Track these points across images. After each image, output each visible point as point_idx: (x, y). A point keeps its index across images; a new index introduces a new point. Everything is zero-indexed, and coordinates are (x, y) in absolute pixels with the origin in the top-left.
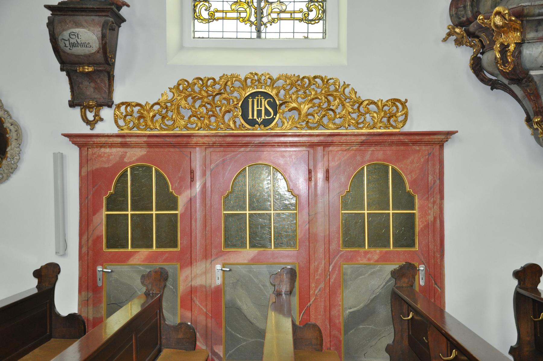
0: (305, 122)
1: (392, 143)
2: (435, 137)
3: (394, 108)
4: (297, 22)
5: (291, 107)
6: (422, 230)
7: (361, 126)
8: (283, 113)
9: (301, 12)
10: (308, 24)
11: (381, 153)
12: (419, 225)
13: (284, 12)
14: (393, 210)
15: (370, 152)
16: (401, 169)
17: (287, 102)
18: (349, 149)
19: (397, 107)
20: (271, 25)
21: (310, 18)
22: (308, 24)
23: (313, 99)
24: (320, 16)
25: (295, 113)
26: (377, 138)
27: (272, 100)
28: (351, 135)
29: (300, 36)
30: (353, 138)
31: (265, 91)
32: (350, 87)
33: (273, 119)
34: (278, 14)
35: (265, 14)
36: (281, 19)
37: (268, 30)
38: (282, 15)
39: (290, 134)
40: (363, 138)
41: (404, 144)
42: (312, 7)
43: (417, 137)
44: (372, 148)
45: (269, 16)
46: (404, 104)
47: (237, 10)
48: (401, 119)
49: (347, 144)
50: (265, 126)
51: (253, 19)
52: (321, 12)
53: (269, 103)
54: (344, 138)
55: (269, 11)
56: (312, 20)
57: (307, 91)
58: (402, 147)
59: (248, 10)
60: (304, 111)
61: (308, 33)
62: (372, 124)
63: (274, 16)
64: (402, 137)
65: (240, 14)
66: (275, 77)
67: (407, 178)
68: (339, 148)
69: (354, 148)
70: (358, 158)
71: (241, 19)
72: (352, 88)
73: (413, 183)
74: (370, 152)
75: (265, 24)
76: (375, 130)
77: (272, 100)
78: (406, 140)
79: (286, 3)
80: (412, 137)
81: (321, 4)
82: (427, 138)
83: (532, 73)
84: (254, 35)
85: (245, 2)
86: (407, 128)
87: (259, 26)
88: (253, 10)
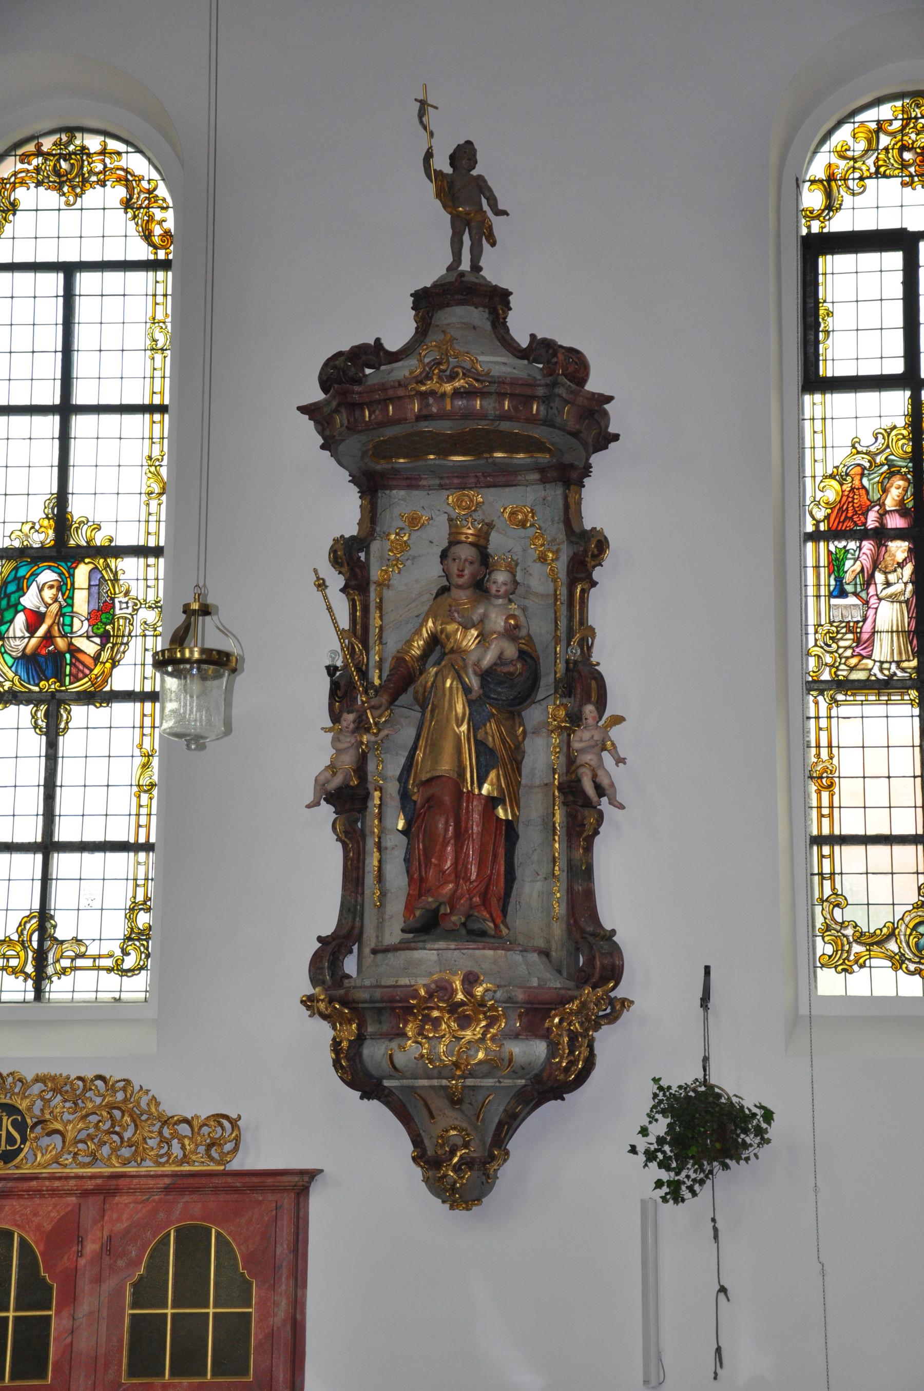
0: (72, 1155)
1: (216, 1190)
2: (285, 1178)
3: (219, 1129)
4: (103, 973)
5: (49, 1130)
6: (259, 1345)
7: (163, 1160)
8: (37, 1139)
9: (111, 956)
10: (121, 976)
11: (200, 1205)
12: (256, 1334)
13: (82, 956)
14: (207, 1306)
15: (180, 1205)
16: (230, 1234)
17: (45, 1121)
18: (147, 1200)
19: (224, 1129)
20: (59, 978)
21: (126, 966)
22: (121, 976)
23: (87, 1115)
24: (142, 963)
25: (57, 1139)
26: (191, 1180)
27: (19, 1118)
28: (145, 1176)
29: (107, 996)
30: (151, 1182)
31: (10, 1102)
32: (150, 1094)
33: (20, 1150)
34: (73, 960)
35: (50, 960)
36: (76, 969)
37: (54, 987)
38: (80, 962)
39: (44, 1175)
40: (167, 1181)
41: (235, 1190)
42: (129, 948)
43: (255, 1180)
44: (186, 1198)
45: (57, 965)
46: (234, 1123)
47: (4, 954)
48: (229, 1147)
49: (143, 1191)
50: (5, 1163)
51: (30, 969)
52: (143, 956)
53: (15, 1124)
54: (136, 1181)
55: (58, 956)
56: (129, 970)
57: (80, 1101)
58: (236, 1196)
59: (22, 954)
60: (70, 1136)
61: (121, 991)
62: (181, 1156)
63: (65, 963)
64: (230, 1180)
65: (8, 961)
66: (30, 1077)
67: (240, 1250)
68: (132, 1198)
69: (156, 1197)
70: (161, 1216)
71: (11, 969)
72: (153, 1096)
73: (249, 1259)
74: (180, 1205)
75: (50, 978)
76: (186, 1168)
77: (19, 1118)
78: (238, 1184)
79: (87, 943)
80: (247, 1179)
81: (145, 943)
82: (270, 1181)
83: (386, 1083)
84: (31, 996)
85: (18, 941)
86: (236, 1164)
87: (40, 979)
88: (30, 954)
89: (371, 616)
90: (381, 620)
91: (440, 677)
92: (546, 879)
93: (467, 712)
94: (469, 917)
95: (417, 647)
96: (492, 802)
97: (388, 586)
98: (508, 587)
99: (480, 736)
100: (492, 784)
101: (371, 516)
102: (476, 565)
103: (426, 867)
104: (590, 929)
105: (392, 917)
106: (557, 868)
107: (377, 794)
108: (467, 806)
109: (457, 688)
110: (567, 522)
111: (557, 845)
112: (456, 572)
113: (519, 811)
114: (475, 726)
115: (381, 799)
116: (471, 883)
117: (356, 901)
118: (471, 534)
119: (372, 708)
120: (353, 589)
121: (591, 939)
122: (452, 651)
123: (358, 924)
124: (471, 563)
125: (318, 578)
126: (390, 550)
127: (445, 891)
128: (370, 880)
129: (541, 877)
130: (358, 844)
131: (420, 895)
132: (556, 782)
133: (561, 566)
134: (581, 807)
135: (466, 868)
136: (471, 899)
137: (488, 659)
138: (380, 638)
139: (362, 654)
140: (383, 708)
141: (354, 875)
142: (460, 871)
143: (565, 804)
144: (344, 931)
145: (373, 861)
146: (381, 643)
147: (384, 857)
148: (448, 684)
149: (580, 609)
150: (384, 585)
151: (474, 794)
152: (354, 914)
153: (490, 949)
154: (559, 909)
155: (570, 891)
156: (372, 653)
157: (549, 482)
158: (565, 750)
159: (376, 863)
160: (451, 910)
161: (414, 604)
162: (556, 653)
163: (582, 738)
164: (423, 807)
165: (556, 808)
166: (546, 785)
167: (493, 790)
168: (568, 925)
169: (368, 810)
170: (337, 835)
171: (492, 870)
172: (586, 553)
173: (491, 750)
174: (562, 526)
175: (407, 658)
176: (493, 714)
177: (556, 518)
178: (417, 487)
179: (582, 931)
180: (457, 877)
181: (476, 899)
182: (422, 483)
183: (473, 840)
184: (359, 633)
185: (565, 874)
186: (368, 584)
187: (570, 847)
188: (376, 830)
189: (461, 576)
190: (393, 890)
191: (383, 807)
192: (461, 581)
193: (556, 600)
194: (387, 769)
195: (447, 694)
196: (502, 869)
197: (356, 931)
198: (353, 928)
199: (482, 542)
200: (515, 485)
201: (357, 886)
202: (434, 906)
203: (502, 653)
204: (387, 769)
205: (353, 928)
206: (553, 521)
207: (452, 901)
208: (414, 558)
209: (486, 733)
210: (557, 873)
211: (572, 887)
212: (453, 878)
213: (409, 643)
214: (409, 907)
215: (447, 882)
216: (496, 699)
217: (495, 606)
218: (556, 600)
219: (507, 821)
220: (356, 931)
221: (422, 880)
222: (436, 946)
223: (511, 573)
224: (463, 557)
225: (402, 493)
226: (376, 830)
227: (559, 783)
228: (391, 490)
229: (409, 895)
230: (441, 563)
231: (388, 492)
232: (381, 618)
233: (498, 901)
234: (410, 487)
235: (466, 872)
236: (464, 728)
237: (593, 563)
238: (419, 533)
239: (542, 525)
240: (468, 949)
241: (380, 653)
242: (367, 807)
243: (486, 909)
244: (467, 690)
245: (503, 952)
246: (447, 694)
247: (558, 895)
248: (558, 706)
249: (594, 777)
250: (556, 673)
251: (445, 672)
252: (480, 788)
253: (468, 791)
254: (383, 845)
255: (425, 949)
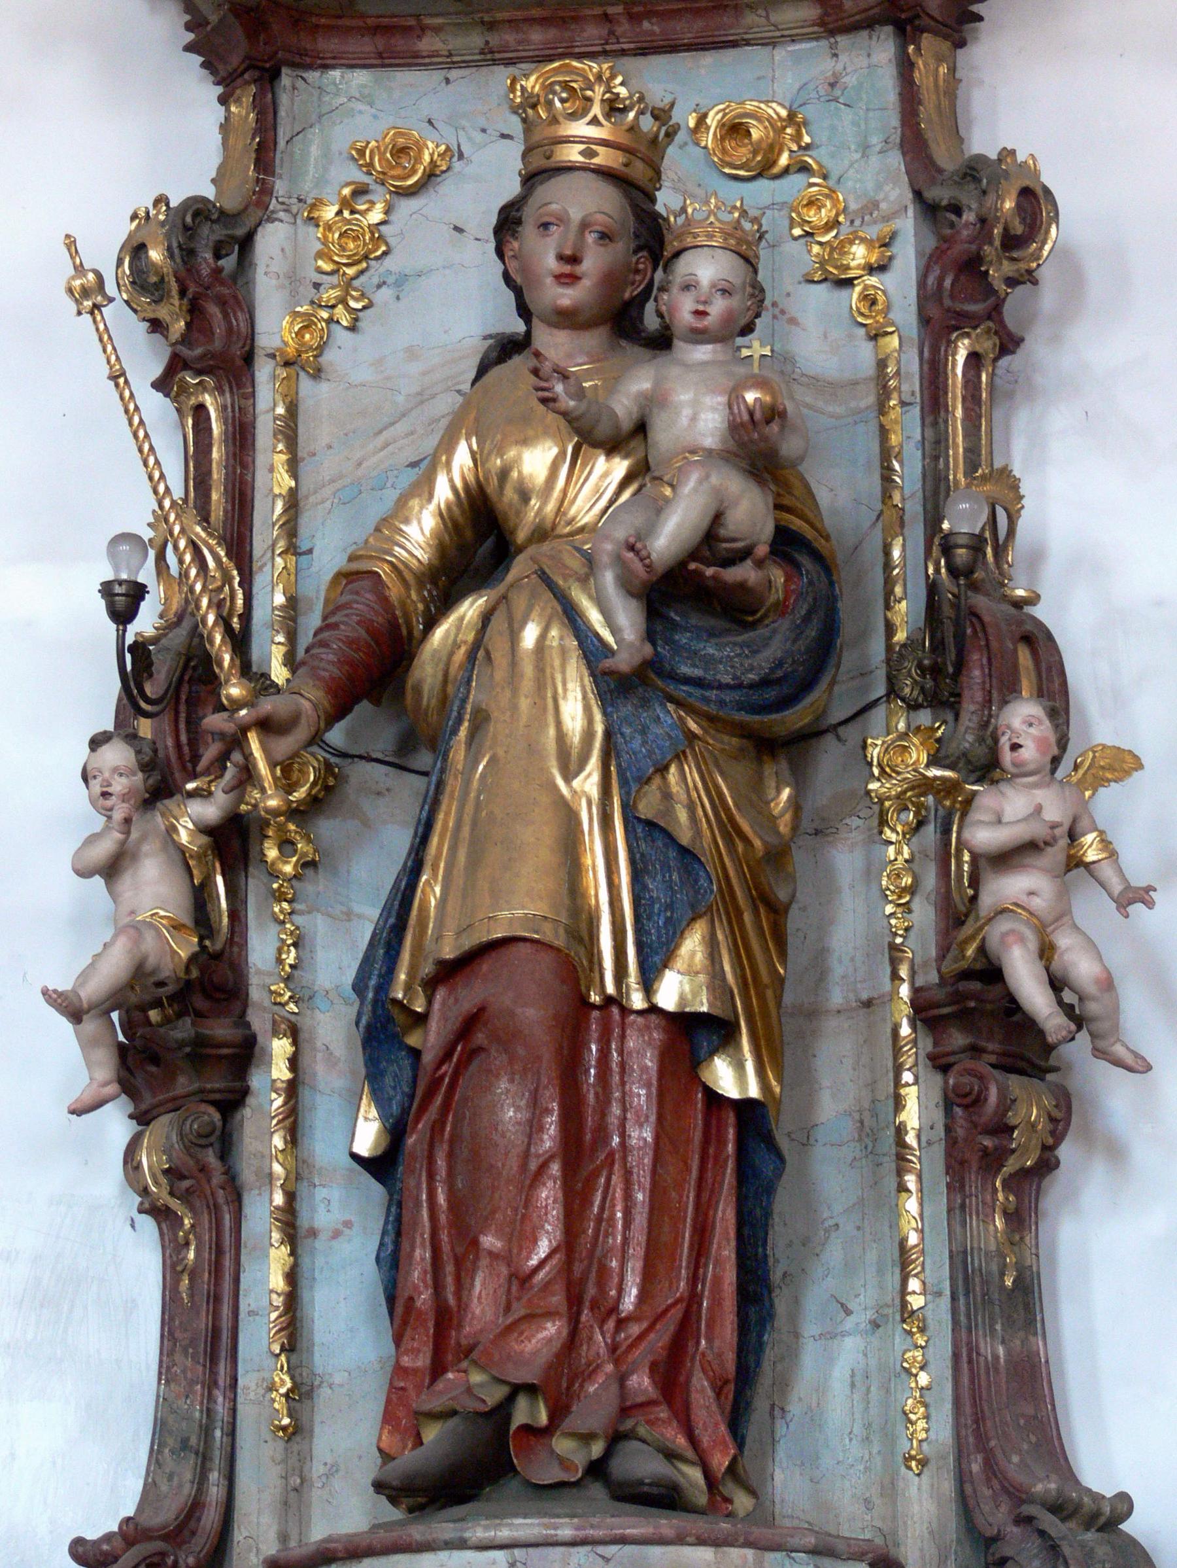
89: (261, 459)
90: (294, 474)
91: (498, 622)
92: (875, 1325)
93: (599, 728)
94: (616, 1438)
95: (419, 535)
96: (691, 1037)
97: (317, 374)
98: (735, 302)
99: (647, 808)
100: (690, 972)
101: (261, 150)
102: (620, 248)
103: (459, 1262)
104: (1045, 1486)
105: (332, 1470)
106: (914, 1284)
107: (281, 1048)
108: (604, 1054)
109: (563, 651)
110: (913, 143)
111: (912, 1205)
112: (551, 262)
113: (780, 1081)
114: (627, 774)
115: (294, 1063)
116: (621, 1323)
117: (210, 1412)
118: (604, 143)
119: (266, 726)
120: (199, 372)
121: (1048, 1521)
122: (542, 534)
123: (215, 1492)
124: (605, 237)
125: (80, 270)
126: (320, 255)
127: (529, 1347)
128: (258, 1338)
129: (861, 1318)
130: (215, 1210)
131: (437, 1369)
132: (905, 991)
133: (900, 286)
134: (1005, 1063)
135: (603, 1270)
136: (622, 1379)
137: (670, 535)
138: (291, 528)
139: (227, 579)
140: (301, 733)
141: (202, 1322)
142: (580, 1285)
143: (940, 1063)
144: (167, 1514)
145: (267, 1272)
146: (292, 549)
147: (305, 1262)
148: (530, 635)
149: (967, 417)
150: (302, 364)
151: (625, 1011)
152: (204, 1459)
153: (701, 1542)
154: (932, 1428)
155: (964, 1357)
156: (260, 582)
157: (851, 28)
158: (930, 880)
159: (277, 1282)
160: (552, 1417)
161: (401, 428)
162: (888, 565)
163: (1004, 814)
164: (447, 1055)
165: (907, 1077)
166: (868, 1004)
167: (695, 994)
168: (962, 1477)
169: (251, 1101)
170: (144, 1192)
171: (694, 1279)
172: (984, 255)
173: (684, 851)
174: (896, 160)
175: (383, 570)
176: (691, 737)
177: (875, 140)
178: (413, 60)
179: (1017, 1495)
180: (575, 1301)
181: (641, 1382)
182: (426, 44)
183: (627, 1174)
184: (222, 502)
185: (945, 1302)
186: (249, 358)
187: (958, 1210)
188: (277, 1169)
189: (569, 279)
190: (338, 1379)
191: (305, 1094)
192: (567, 297)
193: (884, 393)
194: (311, 953)
195: (528, 669)
196: (730, 1276)
197: (210, 1518)
198: (195, 1507)
199: (639, 172)
200: (734, 44)
201: (213, 1359)
202: (494, 1396)
203: (718, 518)
204: (311, 953)
205: (195, 1507)
206: (865, 148)
207: (559, 1385)
208: (401, 281)
209: (667, 796)
210: (916, 1302)
211: (973, 1349)
212: (557, 1299)
213: (389, 525)
214: (401, 1414)
215: (533, 1318)
216: (698, 683)
217: (688, 367)
218: (884, 393)
219: (745, 1107)
220: (210, 1518)
221: (445, 1319)
222: (504, 1534)
223: (747, 260)
224: (576, 215)
225: (360, 77)
226: (277, 1169)
227: (916, 991)
228: (325, 67)
229: (399, 1370)
230: (500, 253)
231: (313, 76)
232: (293, 467)
233: (718, 1394)
234: (385, 60)
235: (601, 1285)
236: (589, 782)
237: (1008, 268)
238: (413, 204)
239: (826, 161)
240: (623, 1540)
241: (293, 578)
242: (245, 1092)
243: (675, 1414)
244: (593, 651)
245: (749, 1553)
246: (528, 669)
247: (924, 1379)
248: (904, 736)
249: (1046, 951)
250: (890, 629)
251: (519, 601)
252: (648, 988)
253: (609, 1001)
254: (304, 1222)
255: (461, 1544)
